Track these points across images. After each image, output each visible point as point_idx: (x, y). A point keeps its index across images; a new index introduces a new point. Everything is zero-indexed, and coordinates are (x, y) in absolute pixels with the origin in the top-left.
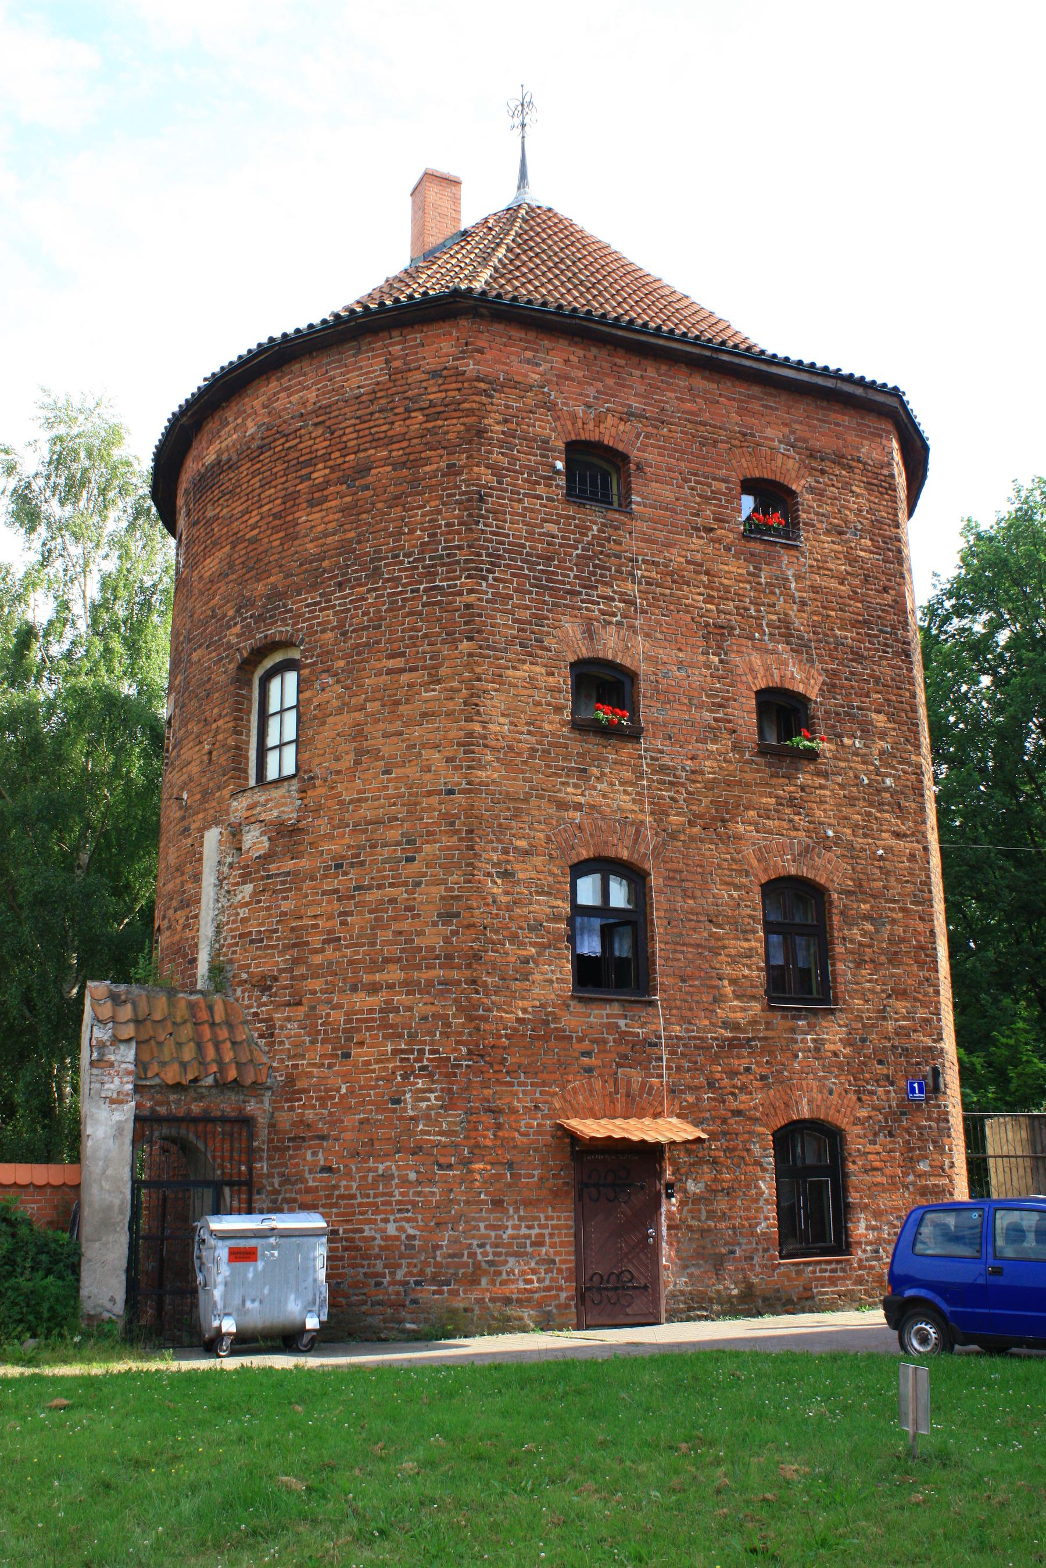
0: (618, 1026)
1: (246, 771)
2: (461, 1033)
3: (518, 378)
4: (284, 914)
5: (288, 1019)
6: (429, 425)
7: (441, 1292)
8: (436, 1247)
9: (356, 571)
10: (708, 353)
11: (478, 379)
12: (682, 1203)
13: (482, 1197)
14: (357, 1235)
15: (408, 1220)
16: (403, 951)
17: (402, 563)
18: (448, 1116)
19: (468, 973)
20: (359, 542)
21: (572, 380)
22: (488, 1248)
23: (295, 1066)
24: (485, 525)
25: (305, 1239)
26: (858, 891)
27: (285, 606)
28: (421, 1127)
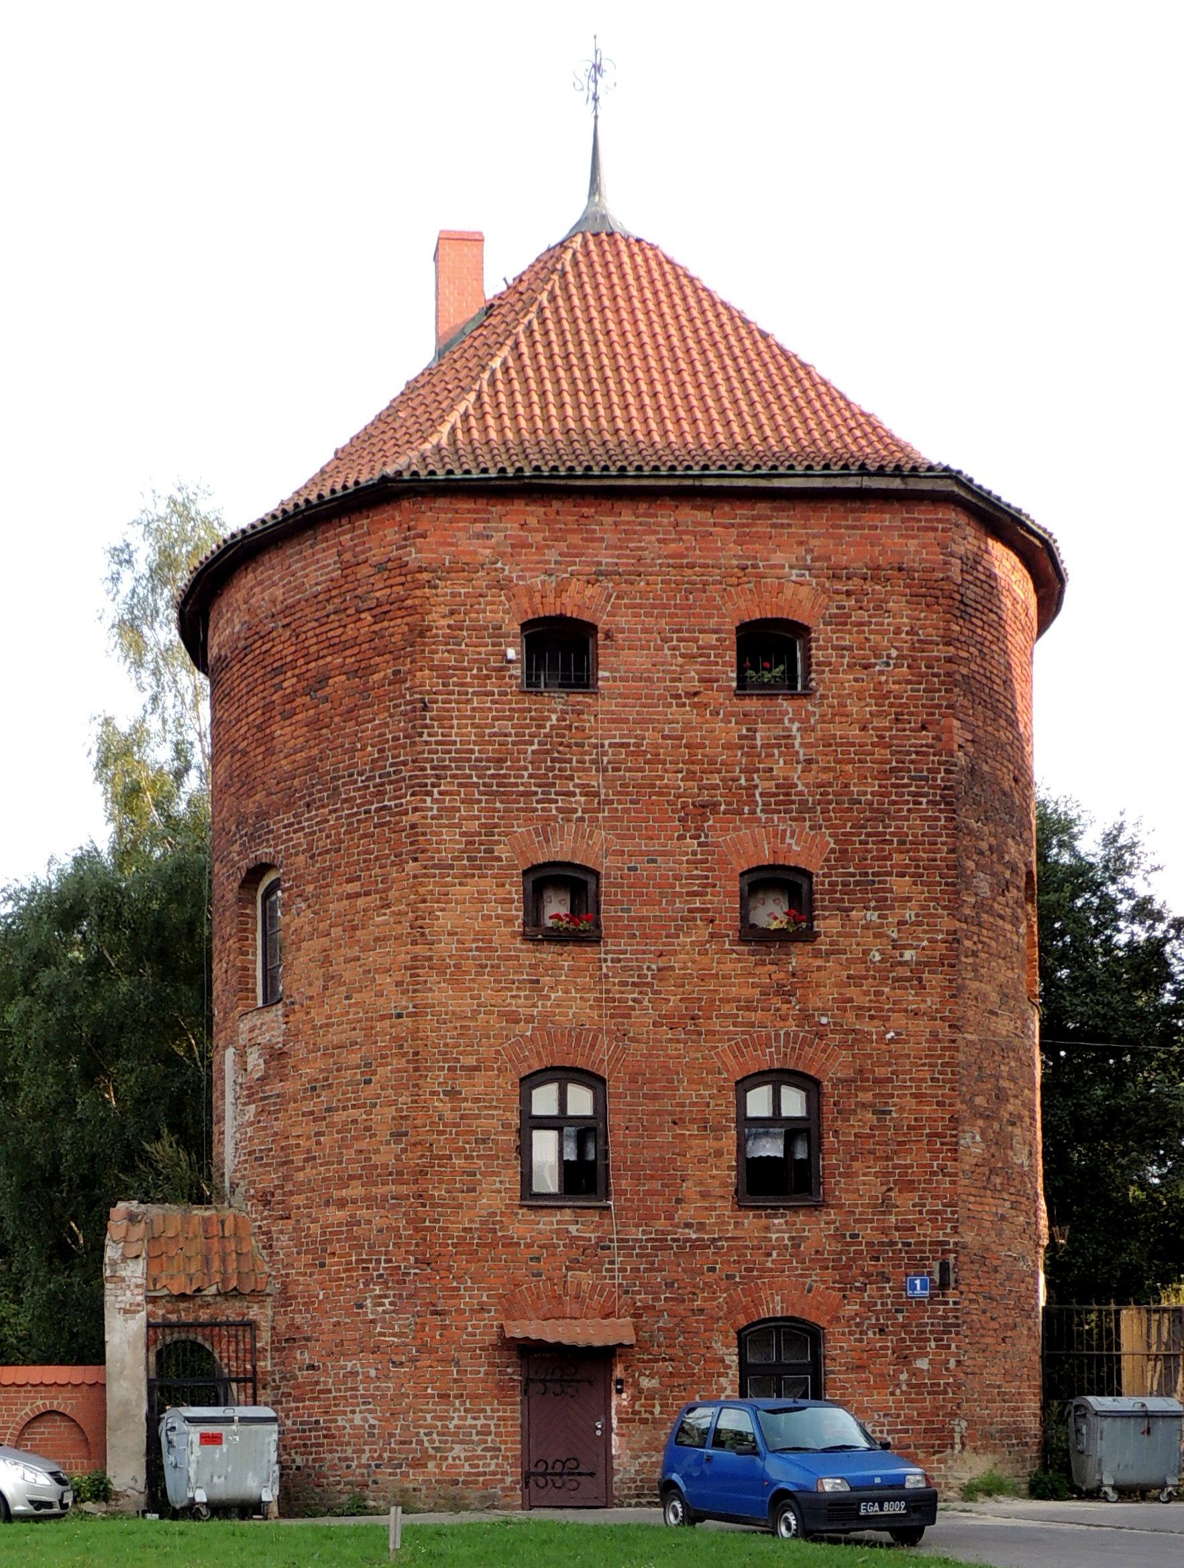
0: (568, 1232)
1: (254, 991)
2: (409, 1244)
3: (467, 559)
4: (276, 1134)
5: (281, 1232)
6: (377, 627)
7: (394, 1474)
8: (391, 1435)
9: (320, 791)
10: (689, 482)
11: (421, 570)
12: (634, 1399)
13: (429, 1391)
14: (333, 1425)
15: (370, 1411)
16: (363, 1168)
17: (356, 782)
18: (399, 1319)
19: (415, 1187)
20: (321, 760)
21: (531, 546)
22: (435, 1436)
23: (287, 1275)
24: (429, 735)
26: (859, 1079)
27: (268, 826)
28: (378, 1329)
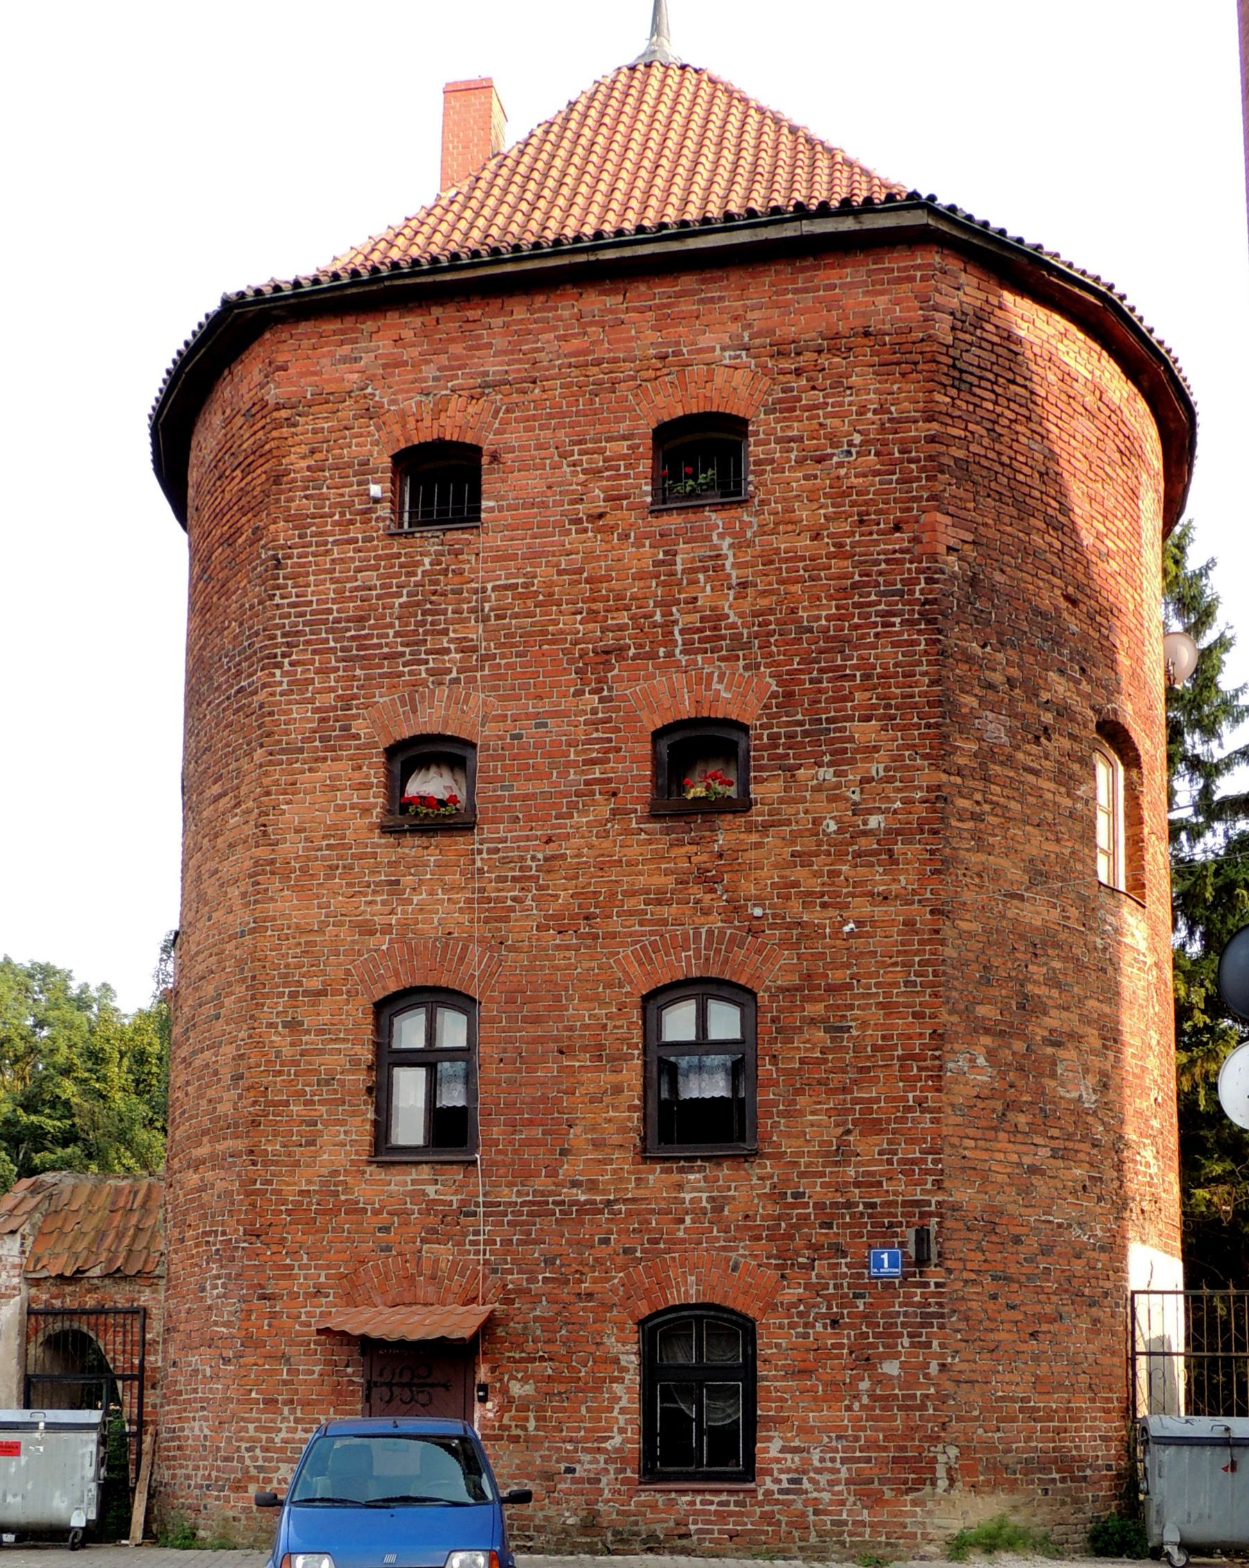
0: (424, 1193)
10: (582, 258)
12: (502, 1409)
13: (253, 1395)
21: (405, 364)
22: (258, 1451)
25: (64, 1436)
